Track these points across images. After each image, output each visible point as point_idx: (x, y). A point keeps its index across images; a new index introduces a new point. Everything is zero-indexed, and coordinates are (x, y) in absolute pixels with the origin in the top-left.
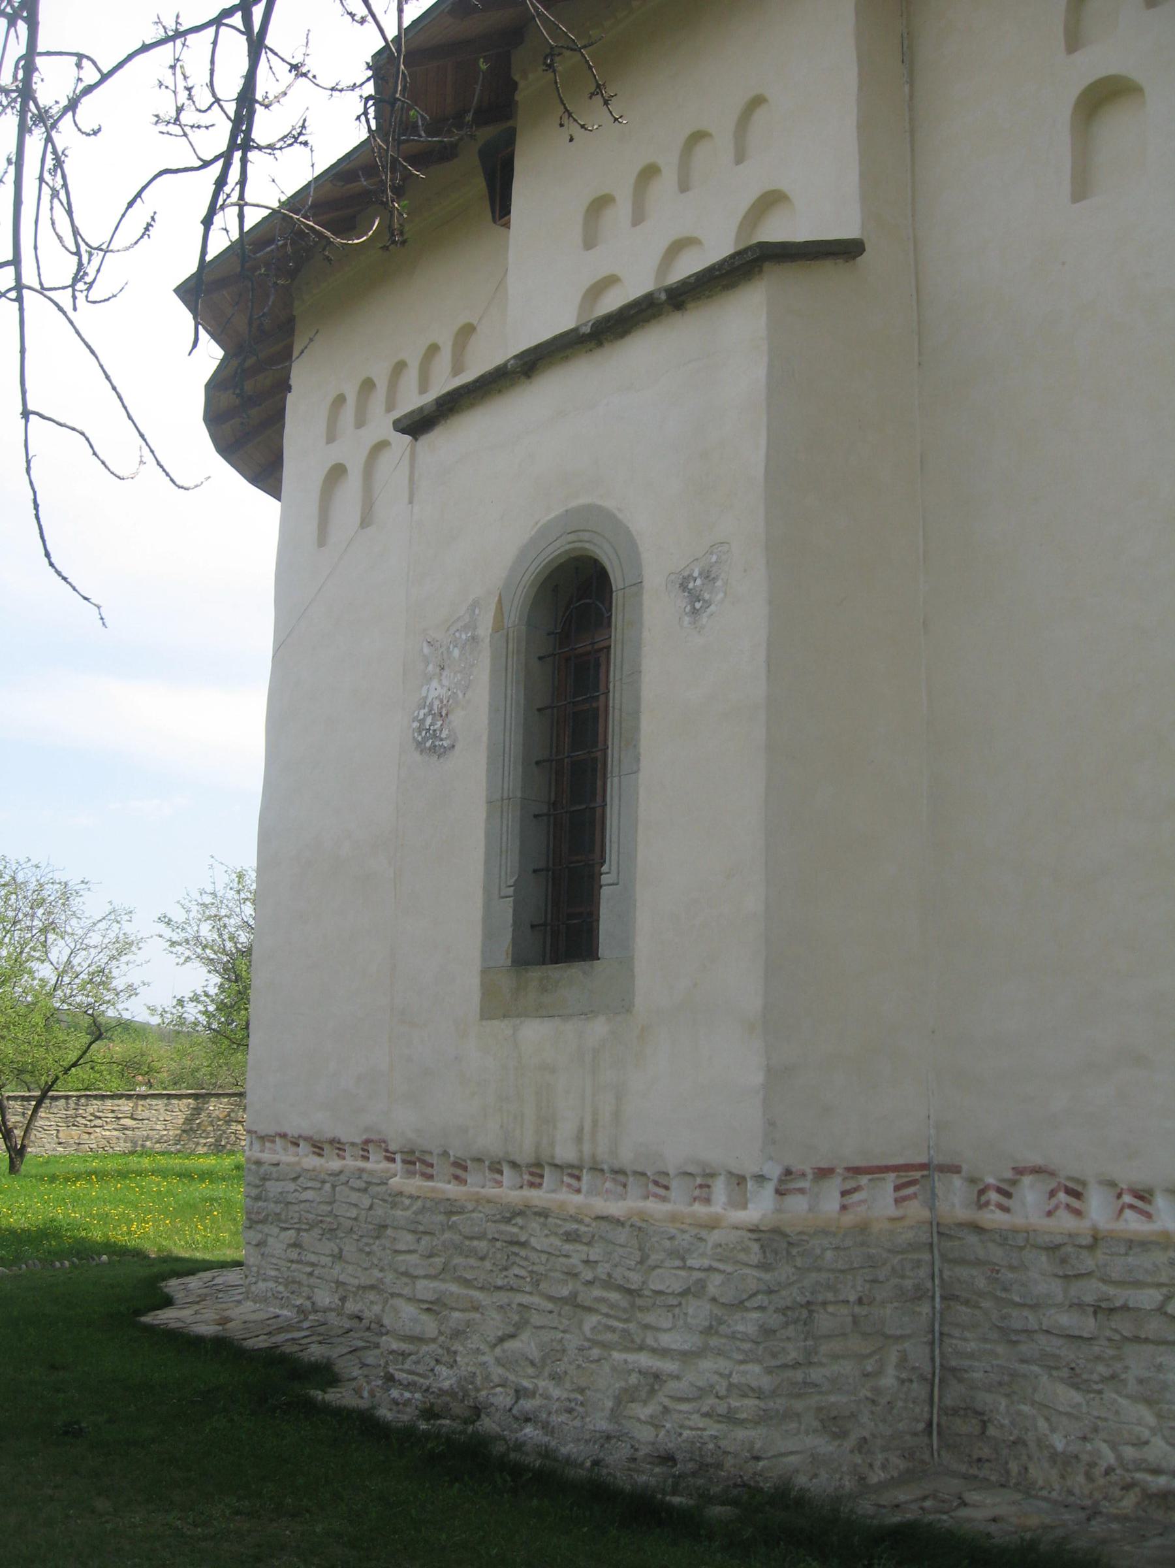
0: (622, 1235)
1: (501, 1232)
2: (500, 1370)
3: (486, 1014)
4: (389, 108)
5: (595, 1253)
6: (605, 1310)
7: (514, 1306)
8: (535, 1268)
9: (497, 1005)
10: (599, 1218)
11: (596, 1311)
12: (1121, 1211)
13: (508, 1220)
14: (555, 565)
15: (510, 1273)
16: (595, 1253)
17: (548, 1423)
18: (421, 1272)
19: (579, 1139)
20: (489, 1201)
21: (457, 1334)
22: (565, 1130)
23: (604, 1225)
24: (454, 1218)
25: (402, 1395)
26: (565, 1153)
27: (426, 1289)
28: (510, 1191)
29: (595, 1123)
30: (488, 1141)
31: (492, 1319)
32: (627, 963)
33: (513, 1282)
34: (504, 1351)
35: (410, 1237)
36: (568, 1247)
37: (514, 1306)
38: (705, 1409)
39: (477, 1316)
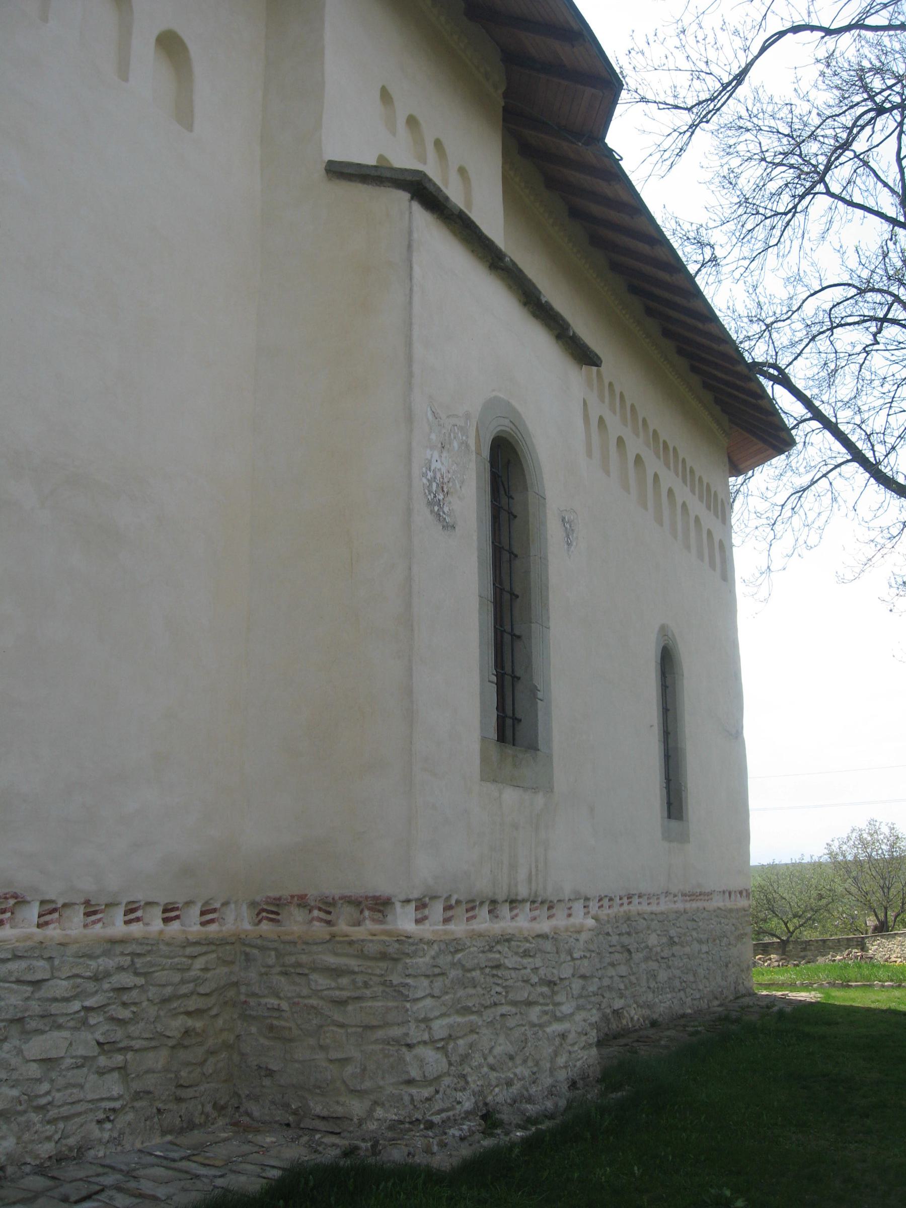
0: (548, 946)
1: (489, 960)
2: (495, 1074)
3: (482, 780)
4: (891, 332)
5: (538, 962)
6: (541, 1001)
7: (498, 1018)
8: (508, 983)
9: (491, 773)
10: (538, 936)
11: (536, 1003)
12: (260, 921)
13: (491, 950)
14: (511, 440)
15: (493, 992)
16: (538, 962)
17: (530, 1096)
18: (437, 1013)
19: (530, 881)
20: (480, 935)
21: (465, 1058)
22: (522, 874)
23: (540, 940)
24: (459, 956)
25: (461, 1130)
26: (523, 891)
27: (440, 1028)
28: (483, 923)
29: (537, 867)
30: (482, 885)
31: (484, 1035)
32: (549, 757)
33: (496, 999)
34: (495, 1057)
35: (425, 982)
36: (525, 961)
37: (498, 1018)
38: (582, 1045)
39: (475, 1036)
